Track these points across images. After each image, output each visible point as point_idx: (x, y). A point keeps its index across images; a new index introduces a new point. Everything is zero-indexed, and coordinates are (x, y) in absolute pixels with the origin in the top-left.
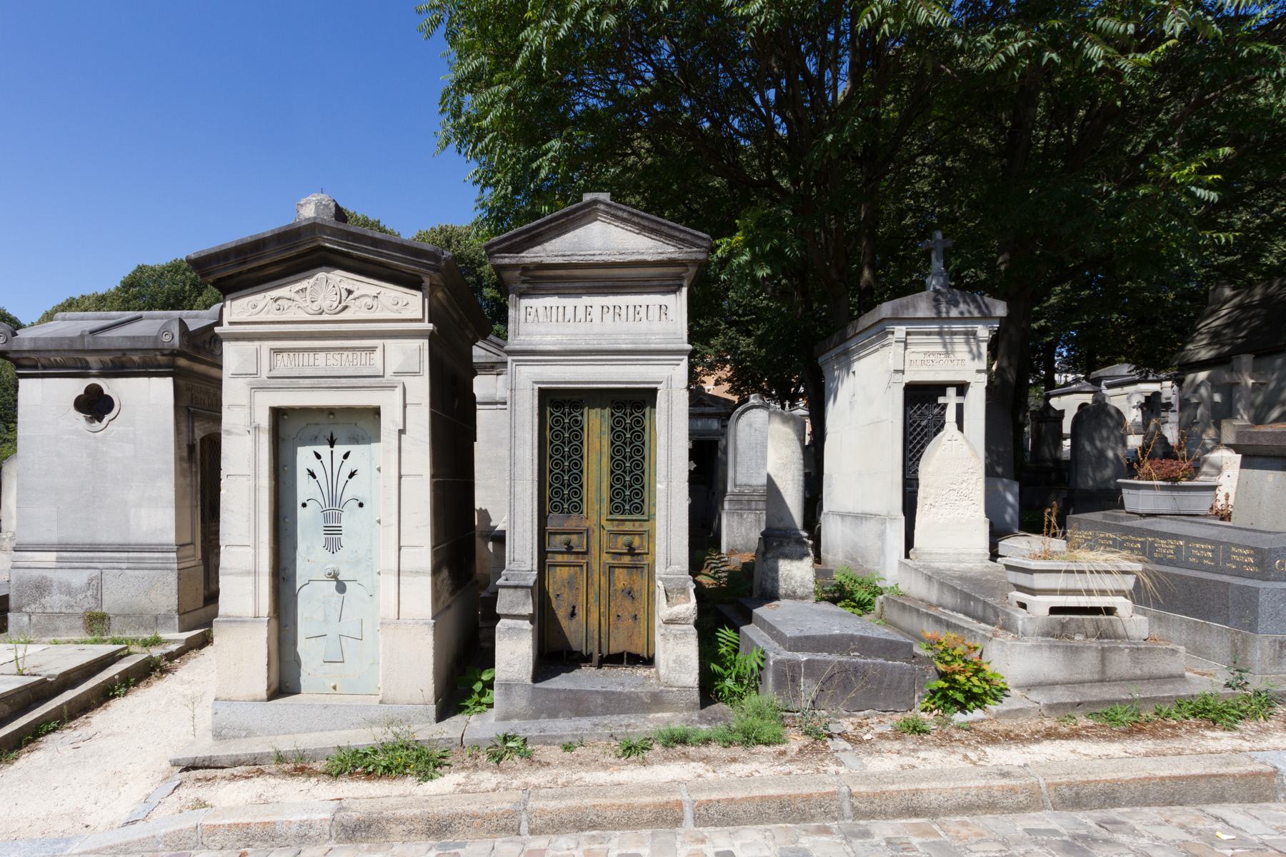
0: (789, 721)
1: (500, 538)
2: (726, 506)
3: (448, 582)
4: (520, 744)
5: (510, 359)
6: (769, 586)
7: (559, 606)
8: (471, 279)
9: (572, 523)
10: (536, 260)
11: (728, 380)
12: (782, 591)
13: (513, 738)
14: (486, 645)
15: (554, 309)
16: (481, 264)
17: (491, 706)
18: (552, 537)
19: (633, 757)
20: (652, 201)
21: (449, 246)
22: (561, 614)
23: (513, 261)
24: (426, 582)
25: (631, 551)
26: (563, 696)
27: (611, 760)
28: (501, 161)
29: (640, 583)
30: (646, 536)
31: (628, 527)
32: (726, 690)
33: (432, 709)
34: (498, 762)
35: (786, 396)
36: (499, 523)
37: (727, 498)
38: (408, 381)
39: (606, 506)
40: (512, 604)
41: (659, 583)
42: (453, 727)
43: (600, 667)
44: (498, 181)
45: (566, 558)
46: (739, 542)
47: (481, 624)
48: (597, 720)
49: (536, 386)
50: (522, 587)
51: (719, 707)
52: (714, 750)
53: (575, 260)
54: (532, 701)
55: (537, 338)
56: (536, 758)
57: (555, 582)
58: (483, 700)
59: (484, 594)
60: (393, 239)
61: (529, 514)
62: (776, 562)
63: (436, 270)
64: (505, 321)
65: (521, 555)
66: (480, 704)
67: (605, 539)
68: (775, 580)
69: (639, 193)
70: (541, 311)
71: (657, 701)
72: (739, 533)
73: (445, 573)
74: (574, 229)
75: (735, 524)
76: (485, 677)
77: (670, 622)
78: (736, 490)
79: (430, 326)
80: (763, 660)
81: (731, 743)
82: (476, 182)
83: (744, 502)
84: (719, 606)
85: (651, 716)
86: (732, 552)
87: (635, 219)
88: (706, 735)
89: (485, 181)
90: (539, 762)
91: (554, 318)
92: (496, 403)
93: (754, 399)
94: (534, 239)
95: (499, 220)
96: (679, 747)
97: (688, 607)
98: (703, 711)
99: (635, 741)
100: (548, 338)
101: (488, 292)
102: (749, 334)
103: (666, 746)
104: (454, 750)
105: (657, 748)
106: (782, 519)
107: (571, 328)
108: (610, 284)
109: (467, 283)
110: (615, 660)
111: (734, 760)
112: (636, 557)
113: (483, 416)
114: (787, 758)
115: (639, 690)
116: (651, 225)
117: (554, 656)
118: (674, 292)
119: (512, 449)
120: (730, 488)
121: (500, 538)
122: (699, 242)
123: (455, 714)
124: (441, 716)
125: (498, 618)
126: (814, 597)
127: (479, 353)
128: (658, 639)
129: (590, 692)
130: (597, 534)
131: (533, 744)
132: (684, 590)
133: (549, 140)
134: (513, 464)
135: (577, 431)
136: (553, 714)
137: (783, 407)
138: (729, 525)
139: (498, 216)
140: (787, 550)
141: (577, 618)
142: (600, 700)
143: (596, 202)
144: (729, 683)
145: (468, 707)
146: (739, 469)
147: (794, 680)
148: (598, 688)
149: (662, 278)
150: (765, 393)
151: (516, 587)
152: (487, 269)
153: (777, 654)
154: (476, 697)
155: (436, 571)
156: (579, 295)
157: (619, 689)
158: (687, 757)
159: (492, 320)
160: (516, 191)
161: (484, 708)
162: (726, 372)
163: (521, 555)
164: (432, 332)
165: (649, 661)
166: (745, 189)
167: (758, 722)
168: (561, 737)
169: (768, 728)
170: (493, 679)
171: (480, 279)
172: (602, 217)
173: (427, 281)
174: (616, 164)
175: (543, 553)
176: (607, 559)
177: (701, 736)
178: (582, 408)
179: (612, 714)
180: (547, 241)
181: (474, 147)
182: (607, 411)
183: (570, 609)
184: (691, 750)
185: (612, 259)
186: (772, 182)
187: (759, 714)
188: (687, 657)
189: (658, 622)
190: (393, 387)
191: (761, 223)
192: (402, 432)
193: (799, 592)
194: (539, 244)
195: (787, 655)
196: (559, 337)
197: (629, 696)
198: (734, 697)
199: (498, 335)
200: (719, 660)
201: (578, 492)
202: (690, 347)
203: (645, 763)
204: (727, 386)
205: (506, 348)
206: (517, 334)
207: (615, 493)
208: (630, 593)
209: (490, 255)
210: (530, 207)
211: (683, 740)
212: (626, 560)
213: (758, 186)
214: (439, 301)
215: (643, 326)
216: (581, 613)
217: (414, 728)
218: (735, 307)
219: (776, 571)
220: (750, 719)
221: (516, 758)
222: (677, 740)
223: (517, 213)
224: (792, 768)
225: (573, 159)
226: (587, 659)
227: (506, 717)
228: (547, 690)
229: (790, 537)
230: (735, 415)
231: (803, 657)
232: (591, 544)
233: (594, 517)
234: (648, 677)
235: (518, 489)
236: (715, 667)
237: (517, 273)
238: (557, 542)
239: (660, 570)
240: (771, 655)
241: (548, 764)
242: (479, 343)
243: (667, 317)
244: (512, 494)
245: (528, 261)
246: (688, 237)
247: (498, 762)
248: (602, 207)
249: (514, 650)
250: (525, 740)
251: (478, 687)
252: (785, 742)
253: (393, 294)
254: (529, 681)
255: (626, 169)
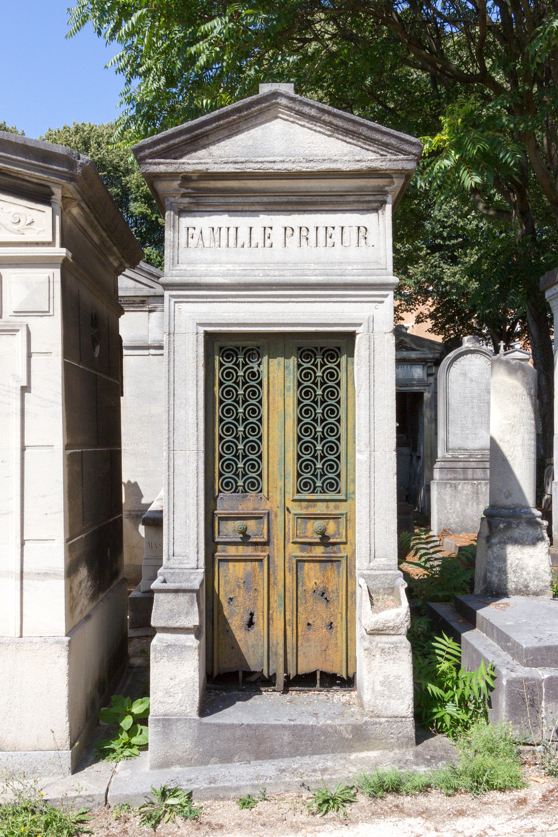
0: (528, 757)
1: (155, 522)
2: (437, 474)
3: (87, 584)
4: (183, 800)
5: (167, 294)
6: (495, 579)
7: (232, 614)
8: (114, 190)
9: (249, 504)
10: (199, 167)
11: (432, 316)
12: (511, 586)
13: (174, 792)
14: (137, 661)
15: (224, 231)
16: (128, 172)
17: (144, 747)
18: (223, 523)
19: (332, 814)
20: (351, 90)
21: (87, 150)
22: (236, 623)
23: (171, 169)
24: (59, 586)
25: (325, 540)
26: (239, 733)
27: (303, 818)
28: (151, 45)
29: (335, 580)
30: (343, 520)
31: (321, 508)
32: (447, 719)
33: (67, 755)
34: (154, 827)
35: (501, 336)
36: (154, 499)
37: (437, 465)
38: (34, 322)
39: (291, 483)
40: (172, 614)
41: (361, 581)
42: (95, 779)
43: (285, 691)
44: (149, 70)
45: (241, 551)
46: (453, 521)
47: (131, 633)
48: (283, 763)
49: (202, 330)
50: (185, 591)
51: (439, 741)
52: (435, 800)
53: (250, 168)
54: (199, 741)
55: (202, 268)
56: (205, 819)
57: (227, 582)
58: (134, 740)
59: (135, 593)
60: (12, 138)
61: (193, 494)
62: (504, 549)
63: (71, 179)
64: (159, 243)
65: (183, 549)
66: (129, 745)
67: (291, 524)
68: (503, 571)
69: (321, 87)
70: (207, 233)
71: (362, 736)
72: (455, 510)
73: (83, 572)
74: (248, 129)
75: (447, 498)
76: (137, 708)
77: (375, 632)
78: (448, 456)
79: (62, 252)
80: (493, 678)
81: (456, 790)
82: (122, 70)
83: (459, 469)
84: (435, 606)
85: (353, 756)
86: (445, 532)
87: (326, 117)
88: (425, 780)
89: (133, 69)
90: (209, 824)
91: (224, 242)
92: (148, 348)
93: (468, 342)
94: (196, 141)
95: (149, 118)
96: (390, 798)
97: (399, 612)
98: (420, 748)
99: (334, 791)
100: (216, 268)
101: (137, 207)
102: (454, 261)
103: (373, 796)
104: (96, 811)
105: (362, 799)
106: (509, 495)
107: (245, 255)
108: (294, 199)
109: (111, 197)
110: (305, 681)
111: (461, 813)
112: (330, 548)
113: (132, 364)
114: (528, 808)
115: (338, 722)
116: (350, 126)
117: (227, 680)
118: (376, 210)
119: (171, 409)
120: (441, 452)
121: (155, 522)
122: (406, 147)
123: (96, 761)
124: (78, 765)
125: (153, 631)
126: (550, 592)
127: (127, 284)
128: (360, 654)
129: (275, 727)
130: (280, 518)
131: (201, 799)
132: (392, 590)
133: (211, 18)
134: (171, 429)
135: (254, 385)
136: (226, 758)
137: (497, 351)
138: (441, 499)
139: (148, 114)
140: (516, 533)
141: (255, 628)
142: (287, 737)
143: (275, 95)
144: (451, 709)
145: (114, 751)
146: (451, 429)
147: (534, 704)
148: (285, 721)
149: (361, 192)
150: (477, 333)
151: (176, 591)
152: (134, 179)
153: (512, 671)
154: (124, 737)
155: (71, 571)
156: (255, 213)
157: (312, 721)
158: (402, 811)
159: (142, 242)
160: (171, 82)
161: (135, 750)
162: (427, 307)
163: (183, 549)
164: (65, 260)
165: (349, 682)
166: (450, 82)
167: (490, 761)
168: (238, 788)
169: (503, 769)
170: (147, 711)
171: (126, 191)
172: (284, 113)
173: (58, 193)
174: (296, 51)
175: (211, 544)
176: (294, 551)
177: (418, 781)
178: (260, 356)
179: (303, 754)
180: (213, 143)
181: (117, 27)
182: (292, 361)
183: (247, 617)
184: (406, 801)
185: (296, 167)
186: (485, 77)
187: (491, 750)
188: (398, 677)
189: (359, 632)
190: (13, 331)
191: (472, 122)
192: (25, 389)
193: (533, 586)
194: (204, 147)
195: (523, 672)
196: (230, 267)
197: (324, 731)
198: (459, 727)
199: (149, 261)
200: (438, 679)
201: (255, 465)
202: (395, 280)
203: (346, 821)
204: (429, 323)
205: (162, 280)
206: (176, 262)
207: (304, 465)
208: (323, 595)
209: (141, 161)
210: (188, 103)
211: (395, 788)
212: (319, 551)
213: (468, 80)
214: (74, 219)
215: (337, 253)
216: (260, 622)
217: (43, 781)
218: (438, 229)
219: (504, 559)
220: (479, 757)
221: (179, 819)
222: (388, 788)
223: (173, 110)
224: (537, 821)
225: (240, 44)
226: (269, 682)
227: (164, 764)
228: (219, 726)
229: (520, 517)
230: (445, 362)
231: (544, 674)
232: (274, 531)
233: (277, 496)
234: (347, 704)
235: (179, 462)
236: (433, 688)
237: (176, 184)
238: (229, 530)
239: (361, 564)
240: (504, 672)
241: (221, 827)
242: (127, 272)
243: (365, 241)
244: (171, 468)
245: (189, 168)
246: (393, 141)
247: (154, 827)
248: (284, 101)
249: (174, 673)
250: (190, 795)
251: (127, 723)
252: (524, 785)
253: (14, 209)
254: (194, 715)
255: (306, 58)
